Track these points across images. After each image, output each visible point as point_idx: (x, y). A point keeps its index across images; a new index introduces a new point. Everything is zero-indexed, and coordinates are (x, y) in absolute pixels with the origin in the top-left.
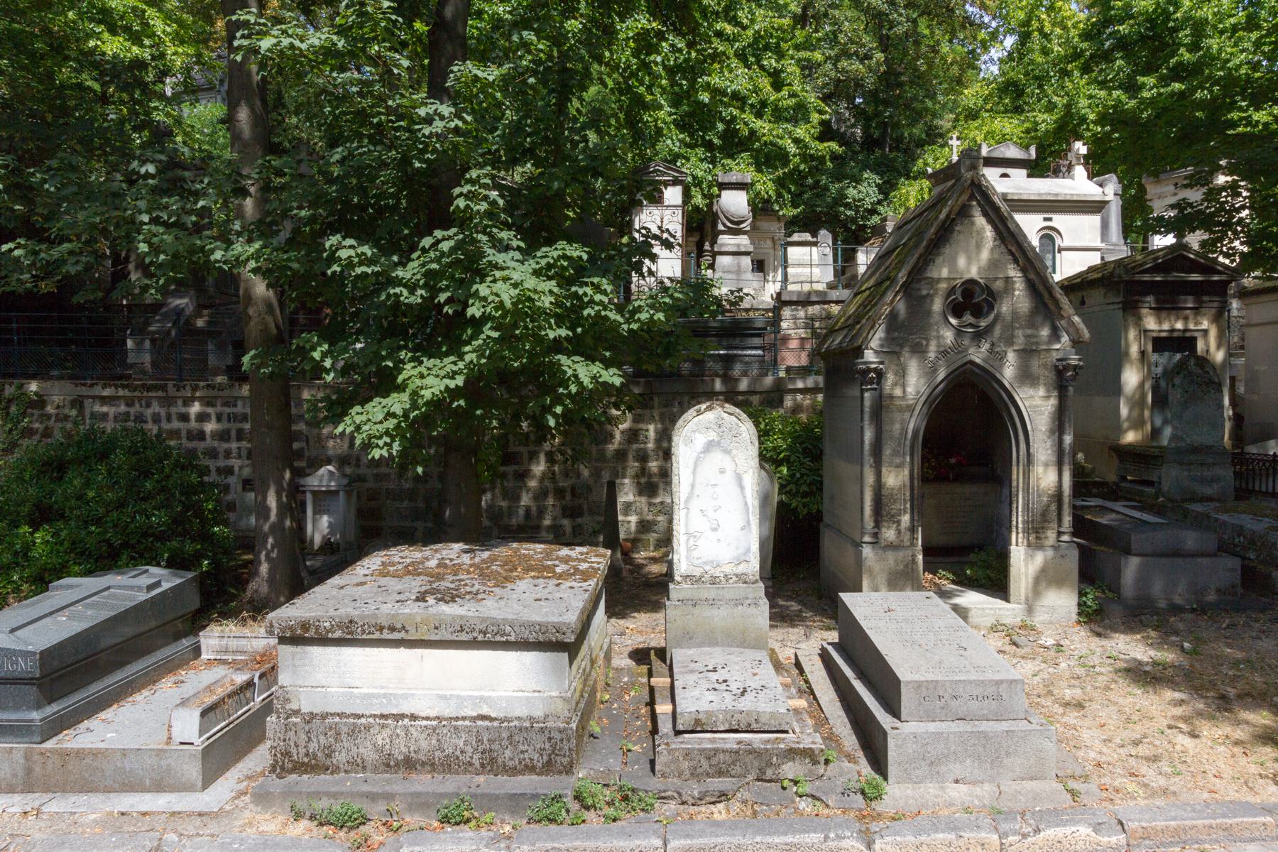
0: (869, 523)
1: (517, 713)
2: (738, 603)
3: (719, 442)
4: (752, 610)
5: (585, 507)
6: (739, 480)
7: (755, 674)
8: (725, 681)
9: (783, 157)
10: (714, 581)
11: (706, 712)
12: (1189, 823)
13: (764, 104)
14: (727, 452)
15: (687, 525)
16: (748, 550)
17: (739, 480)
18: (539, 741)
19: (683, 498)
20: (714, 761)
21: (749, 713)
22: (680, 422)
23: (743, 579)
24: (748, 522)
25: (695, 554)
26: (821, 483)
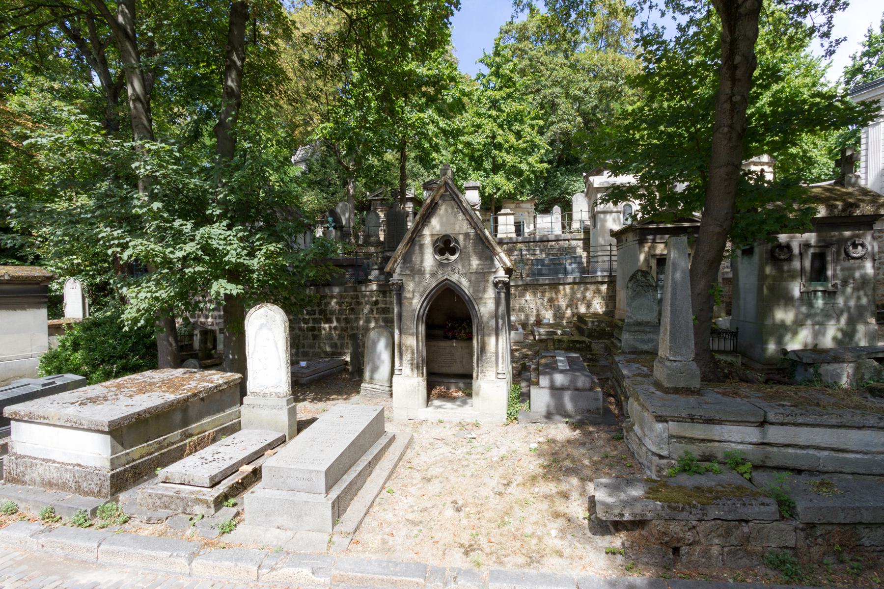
1: (89, 465)
2: (274, 407)
4: (279, 412)
12: (370, 576)
18: (798, 378)
20: (162, 500)
23: (277, 395)
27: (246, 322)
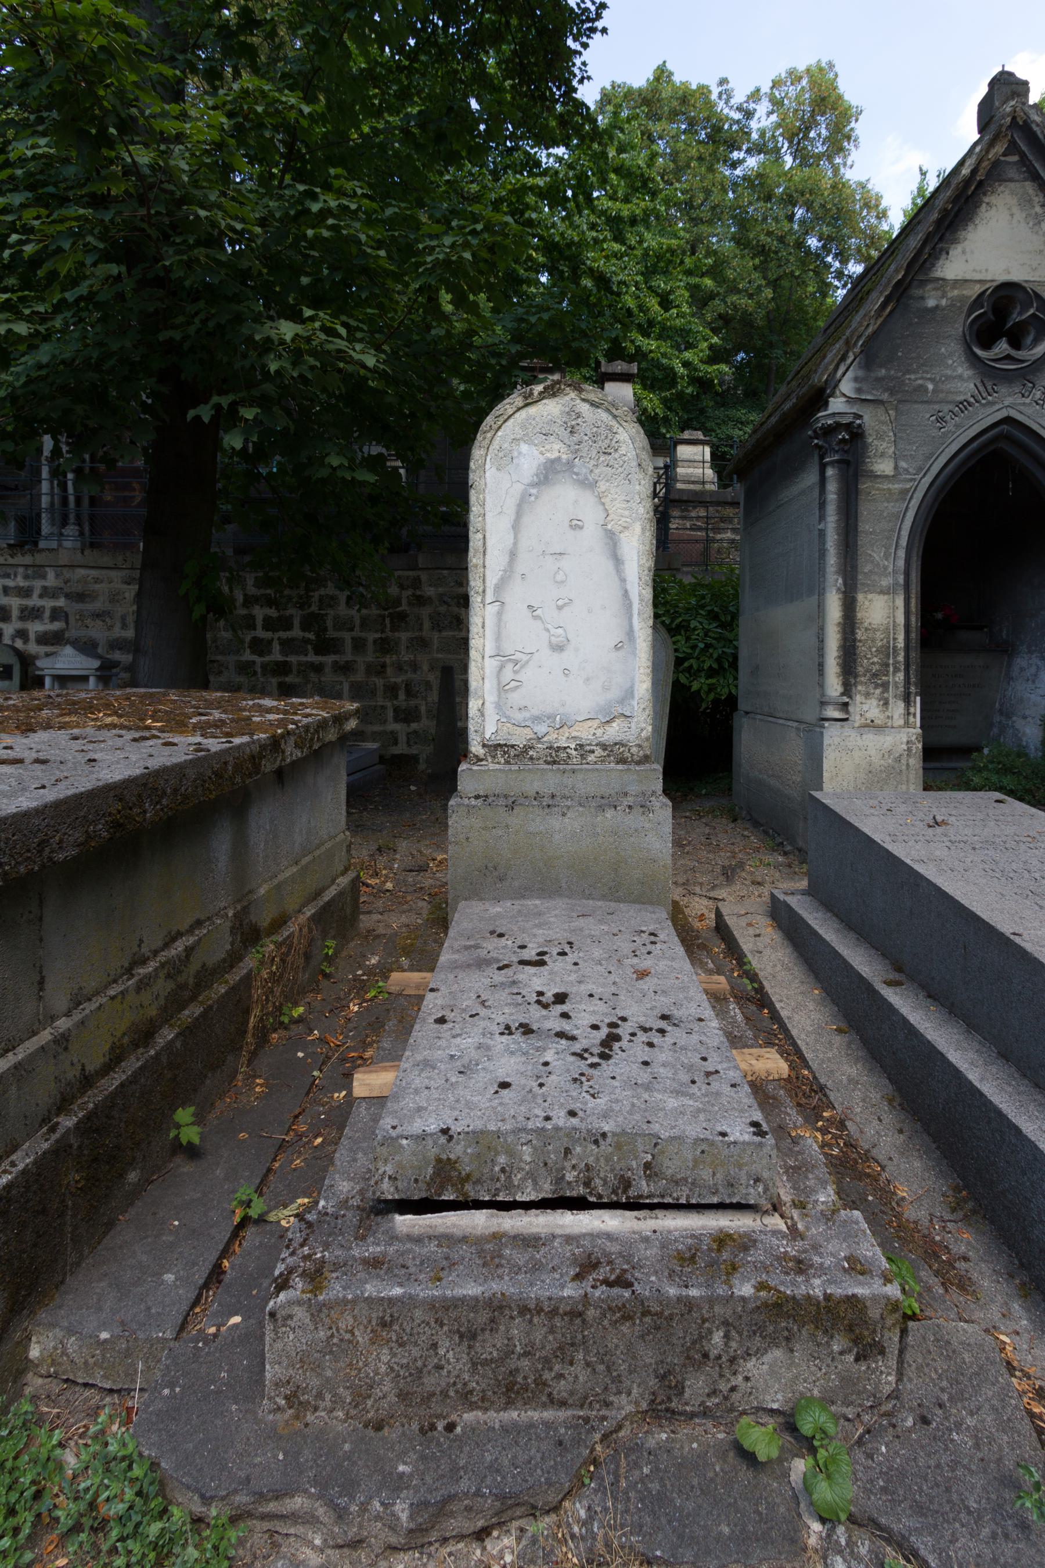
0: (834, 686)
2: (606, 803)
3: (570, 464)
4: (635, 820)
5: (423, 709)
6: (612, 540)
7: (642, 974)
8: (561, 998)
9: (671, 378)
10: (555, 757)
11: (477, 1137)
13: (651, 323)
14: (588, 484)
15: (498, 638)
16: (630, 693)
17: (612, 540)
19: (492, 580)
20: (489, 1347)
21: (623, 1141)
22: (489, 420)
23: (616, 753)
24: (630, 633)
25: (515, 698)
26: (735, 658)
27: (477, 453)
